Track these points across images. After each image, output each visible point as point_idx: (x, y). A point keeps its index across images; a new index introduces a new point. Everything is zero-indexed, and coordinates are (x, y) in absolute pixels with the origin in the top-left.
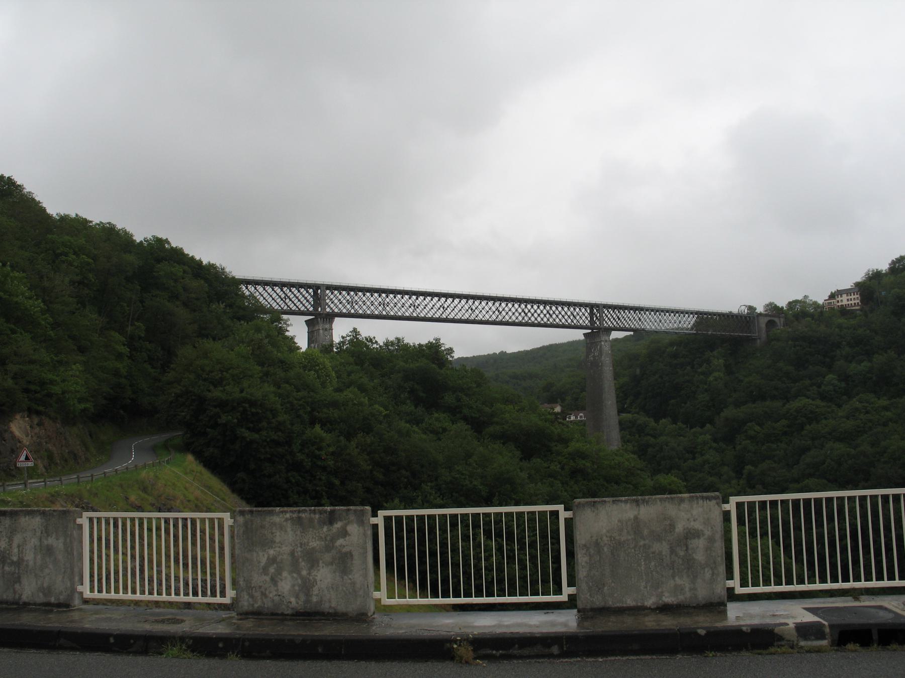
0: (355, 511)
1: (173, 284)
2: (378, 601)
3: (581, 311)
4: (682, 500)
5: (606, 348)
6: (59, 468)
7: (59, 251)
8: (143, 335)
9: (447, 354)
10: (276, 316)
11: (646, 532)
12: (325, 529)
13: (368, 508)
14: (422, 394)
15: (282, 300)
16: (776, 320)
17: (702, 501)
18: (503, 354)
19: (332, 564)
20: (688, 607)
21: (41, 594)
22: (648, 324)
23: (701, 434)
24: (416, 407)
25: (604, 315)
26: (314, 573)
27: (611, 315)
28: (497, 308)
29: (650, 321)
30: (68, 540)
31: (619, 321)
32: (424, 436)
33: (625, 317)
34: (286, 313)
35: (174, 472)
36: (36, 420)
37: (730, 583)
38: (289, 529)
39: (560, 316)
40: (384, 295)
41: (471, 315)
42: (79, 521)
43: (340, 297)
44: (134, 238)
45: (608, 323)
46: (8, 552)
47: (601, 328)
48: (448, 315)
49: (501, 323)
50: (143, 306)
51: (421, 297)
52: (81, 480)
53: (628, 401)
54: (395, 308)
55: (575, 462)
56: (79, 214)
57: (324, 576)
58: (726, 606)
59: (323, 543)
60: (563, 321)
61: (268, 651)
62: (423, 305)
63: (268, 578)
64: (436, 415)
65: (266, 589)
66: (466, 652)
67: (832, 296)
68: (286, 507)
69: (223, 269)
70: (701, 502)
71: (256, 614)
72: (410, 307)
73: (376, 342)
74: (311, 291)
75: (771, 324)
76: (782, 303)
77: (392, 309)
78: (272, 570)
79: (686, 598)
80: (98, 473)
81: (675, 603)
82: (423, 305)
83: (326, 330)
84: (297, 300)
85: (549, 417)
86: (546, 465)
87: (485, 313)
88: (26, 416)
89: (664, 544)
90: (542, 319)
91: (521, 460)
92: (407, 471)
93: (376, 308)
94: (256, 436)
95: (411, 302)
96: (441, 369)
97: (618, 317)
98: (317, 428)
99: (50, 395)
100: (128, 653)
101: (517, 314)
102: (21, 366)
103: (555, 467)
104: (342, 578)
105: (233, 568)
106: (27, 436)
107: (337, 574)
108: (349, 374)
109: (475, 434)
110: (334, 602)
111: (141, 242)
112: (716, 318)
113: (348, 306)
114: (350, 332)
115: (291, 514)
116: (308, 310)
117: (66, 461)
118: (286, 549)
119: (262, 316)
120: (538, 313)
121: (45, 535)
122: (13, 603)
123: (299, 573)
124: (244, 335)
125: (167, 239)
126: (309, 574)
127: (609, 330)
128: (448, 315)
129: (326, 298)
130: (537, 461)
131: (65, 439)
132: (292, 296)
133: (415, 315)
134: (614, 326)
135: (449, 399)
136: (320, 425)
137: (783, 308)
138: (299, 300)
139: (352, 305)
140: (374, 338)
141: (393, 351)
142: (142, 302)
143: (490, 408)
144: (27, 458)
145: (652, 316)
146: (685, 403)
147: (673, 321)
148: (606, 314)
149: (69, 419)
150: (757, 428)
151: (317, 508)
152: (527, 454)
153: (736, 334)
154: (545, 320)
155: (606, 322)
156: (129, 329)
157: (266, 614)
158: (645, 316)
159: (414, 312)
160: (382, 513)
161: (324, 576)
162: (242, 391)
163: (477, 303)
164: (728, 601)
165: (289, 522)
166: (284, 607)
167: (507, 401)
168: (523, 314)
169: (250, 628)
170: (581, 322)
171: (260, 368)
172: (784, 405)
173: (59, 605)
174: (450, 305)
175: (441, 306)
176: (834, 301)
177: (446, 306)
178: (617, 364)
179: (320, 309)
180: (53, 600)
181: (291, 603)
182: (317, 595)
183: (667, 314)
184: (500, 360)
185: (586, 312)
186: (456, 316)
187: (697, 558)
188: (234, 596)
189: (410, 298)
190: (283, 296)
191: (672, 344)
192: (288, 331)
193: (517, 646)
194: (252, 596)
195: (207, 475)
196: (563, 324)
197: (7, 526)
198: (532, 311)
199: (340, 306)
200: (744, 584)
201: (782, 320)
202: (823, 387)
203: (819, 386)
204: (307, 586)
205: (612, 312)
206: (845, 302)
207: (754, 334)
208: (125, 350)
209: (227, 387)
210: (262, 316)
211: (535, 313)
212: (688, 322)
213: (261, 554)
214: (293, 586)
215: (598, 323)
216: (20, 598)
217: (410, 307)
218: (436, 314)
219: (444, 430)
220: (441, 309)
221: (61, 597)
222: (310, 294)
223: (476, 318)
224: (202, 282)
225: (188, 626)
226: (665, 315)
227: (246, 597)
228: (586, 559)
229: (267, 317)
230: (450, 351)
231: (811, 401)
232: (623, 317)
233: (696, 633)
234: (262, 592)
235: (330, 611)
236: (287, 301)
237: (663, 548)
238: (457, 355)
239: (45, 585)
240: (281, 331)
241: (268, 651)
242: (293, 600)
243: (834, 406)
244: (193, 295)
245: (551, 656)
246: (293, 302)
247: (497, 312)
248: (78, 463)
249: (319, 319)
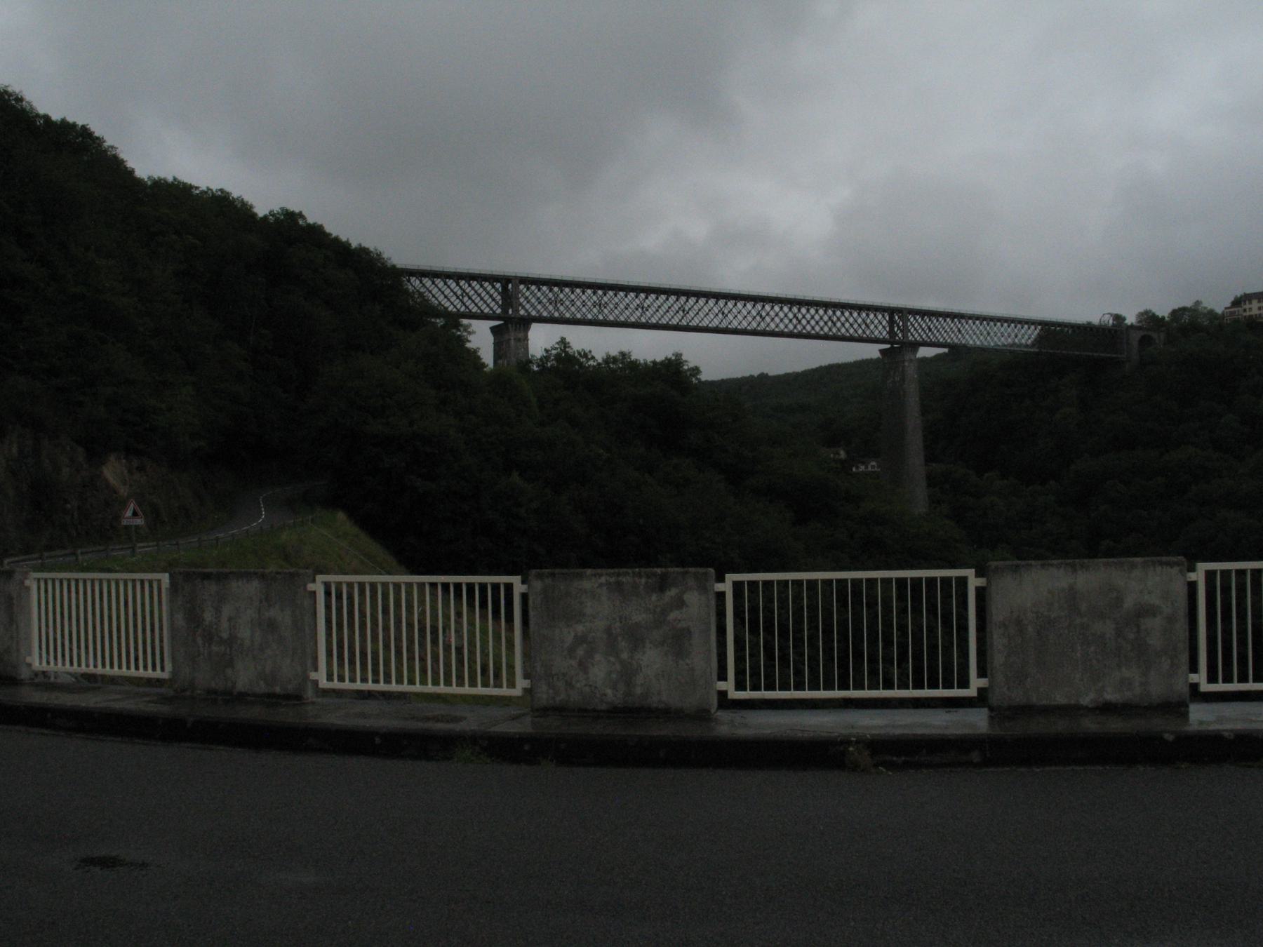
2: (723, 694)
3: (877, 318)
5: (911, 371)
9: (691, 375)
10: (454, 319)
11: (1084, 607)
12: (654, 597)
13: (712, 570)
15: (458, 297)
16: (1154, 335)
17: (1160, 568)
18: (763, 377)
22: (972, 338)
25: (909, 324)
27: (919, 324)
28: (759, 312)
29: (967, 333)
31: (930, 333)
33: (939, 327)
36: (135, 463)
37: (1194, 678)
39: (847, 325)
40: (600, 292)
41: (722, 321)
42: (311, 587)
43: (539, 294)
44: (255, 210)
45: (914, 336)
46: (215, 627)
47: (904, 343)
48: (690, 321)
49: (764, 333)
51: (662, 296)
54: (616, 311)
56: (177, 177)
57: (652, 660)
58: (1187, 706)
59: (651, 616)
60: (852, 331)
62: (672, 311)
63: (574, 663)
67: (1237, 302)
68: (599, 568)
69: (379, 255)
70: (1159, 569)
71: (560, 710)
72: (637, 309)
73: (593, 358)
74: (498, 285)
75: (1145, 341)
76: (1163, 311)
77: (611, 311)
78: (580, 652)
82: (672, 311)
83: (519, 340)
84: (479, 299)
87: (732, 318)
88: (122, 457)
90: (822, 329)
93: (590, 310)
95: (639, 303)
97: (929, 328)
98: (515, 478)
101: (786, 321)
105: (526, 655)
110: (665, 694)
111: (265, 217)
112: (1068, 331)
113: (551, 308)
114: (558, 343)
115: (608, 578)
116: (494, 312)
119: (433, 320)
120: (815, 320)
125: (301, 212)
127: (915, 345)
128: (690, 321)
129: (520, 295)
132: (472, 292)
133: (643, 320)
134: (923, 339)
137: (1163, 318)
138: (482, 299)
139: (556, 306)
140: (590, 352)
144: (135, 514)
145: (978, 326)
147: (1006, 334)
148: (911, 323)
151: (643, 570)
153: (1095, 354)
154: (826, 329)
155: (912, 334)
158: (967, 326)
159: (641, 315)
160: (731, 577)
161: (652, 660)
163: (730, 304)
168: (795, 321)
170: (876, 333)
173: (287, 697)
174: (692, 307)
175: (679, 308)
176: (1240, 309)
177: (687, 309)
179: (510, 311)
180: (278, 690)
181: (605, 695)
183: (999, 324)
184: (758, 385)
185: (884, 319)
186: (700, 322)
188: (527, 687)
189: (637, 297)
190: (459, 292)
192: (469, 341)
196: (851, 335)
198: (808, 316)
199: (539, 307)
200: (1212, 679)
201: (1162, 336)
204: (628, 674)
205: (920, 320)
206: (1255, 312)
207: (1121, 354)
210: (433, 320)
211: (782, 317)
212: (1027, 336)
215: (900, 335)
217: (637, 309)
218: (662, 319)
220: (681, 312)
222: (496, 290)
223: (730, 326)
225: (471, 722)
226: (995, 325)
227: (544, 688)
229: (440, 322)
230: (696, 371)
232: (936, 328)
234: (566, 682)
235: (660, 707)
236: (466, 299)
238: (705, 376)
240: (462, 341)
242: (609, 691)
246: (473, 301)
247: (758, 318)
249: (510, 325)
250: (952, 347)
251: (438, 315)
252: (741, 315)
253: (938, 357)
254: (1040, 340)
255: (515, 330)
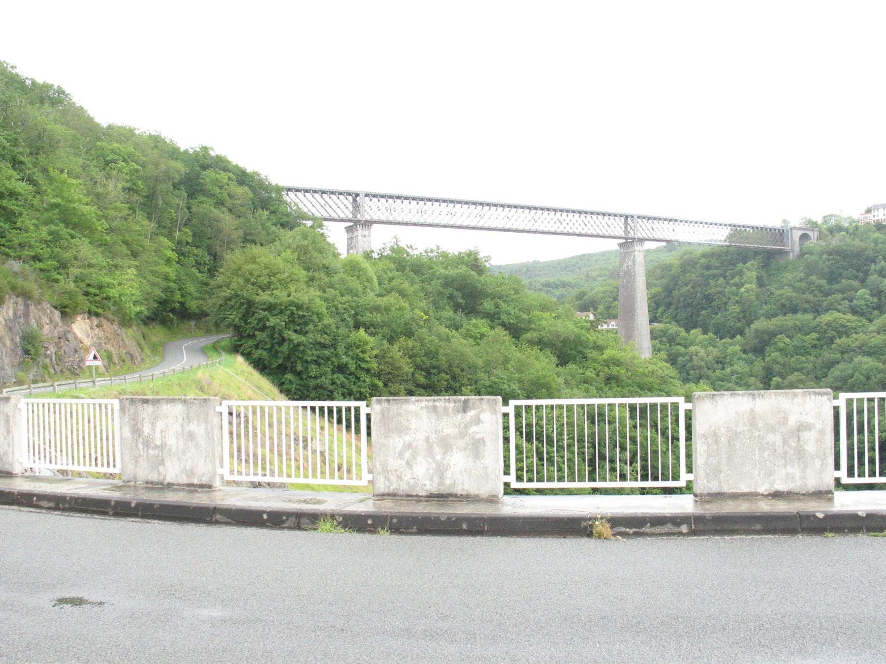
0: (488, 401)
1: (218, 191)
4: (795, 395)
5: (639, 257)
6: (118, 368)
7: (108, 158)
8: (190, 241)
10: (319, 222)
11: (760, 424)
12: (459, 416)
14: (461, 301)
16: (810, 233)
19: (465, 449)
20: (798, 494)
21: (184, 476)
23: (731, 345)
24: (455, 311)
26: (448, 457)
30: (209, 426)
32: (465, 341)
34: (325, 219)
35: (227, 373)
36: (95, 321)
38: (424, 417)
50: (190, 213)
52: (143, 379)
53: (659, 311)
55: (609, 369)
58: (833, 494)
63: (403, 463)
64: (474, 321)
65: (401, 473)
66: (606, 529)
67: (869, 211)
70: (813, 397)
74: (350, 198)
75: (804, 237)
78: (407, 455)
79: (796, 486)
80: (147, 374)
81: (786, 490)
83: (365, 236)
85: (585, 324)
86: (581, 371)
89: (778, 435)
91: (557, 365)
92: (447, 374)
94: (302, 339)
96: (480, 276)
98: (362, 331)
99: (108, 298)
100: (283, 528)
102: (81, 270)
103: (590, 373)
104: (475, 462)
106: (88, 337)
107: (470, 459)
108: (391, 280)
109: (513, 339)
117: (124, 361)
118: (422, 436)
121: (187, 421)
122: (158, 484)
123: (433, 457)
124: (291, 241)
126: (443, 458)
130: (572, 366)
131: (123, 340)
135: (488, 305)
136: (364, 329)
137: (816, 223)
141: (433, 258)
142: (189, 208)
143: (528, 315)
144: (95, 358)
146: (716, 314)
149: (125, 322)
150: (787, 340)
152: (563, 360)
156: (177, 235)
157: (402, 496)
160: (513, 403)
162: (289, 296)
164: (836, 490)
165: (425, 410)
166: (418, 488)
167: (544, 308)
169: (388, 507)
170: (609, 230)
171: (305, 273)
172: (815, 318)
173: (202, 486)
178: (650, 274)
180: (195, 481)
182: (451, 478)
187: (806, 448)
191: (704, 255)
193: (649, 524)
194: (389, 480)
195: (256, 375)
197: (150, 413)
201: (816, 233)
202: (855, 302)
203: (851, 301)
204: (441, 470)
208: (173, 255)
209: (275, 291)
213: (397, 440)
214: (428, 469)
216: (164, 479)
219: (482, 336)
221: (204, 479)
224: (247, 188)
227: (382, 480)
228: (705, 447)
229: (309, 223)
230: (488, 259)
231: (841, 315)
233: (815, 516)
237: (776, 439)
239: (188, 468)
242: (428, 483)
243: (864, 320)
244: (239, 202)
245: (680, 534)
248: (135, 363)
250: (667, 241)
251: (308, 219)
252: (547, 221)
253: (658, 250)
254: (731, 237)
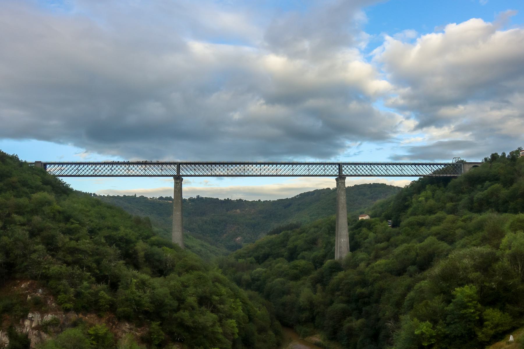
61: (40, 290)
190: (386, 169)
241: (40, 290)
255: (176, 180)
